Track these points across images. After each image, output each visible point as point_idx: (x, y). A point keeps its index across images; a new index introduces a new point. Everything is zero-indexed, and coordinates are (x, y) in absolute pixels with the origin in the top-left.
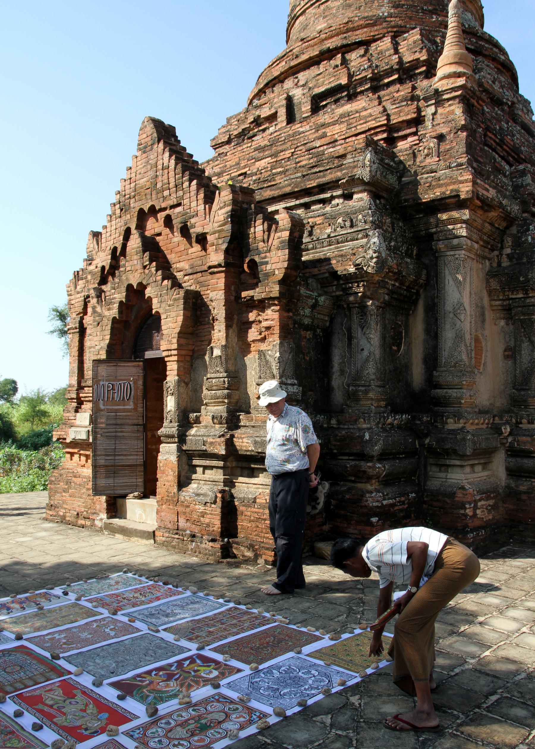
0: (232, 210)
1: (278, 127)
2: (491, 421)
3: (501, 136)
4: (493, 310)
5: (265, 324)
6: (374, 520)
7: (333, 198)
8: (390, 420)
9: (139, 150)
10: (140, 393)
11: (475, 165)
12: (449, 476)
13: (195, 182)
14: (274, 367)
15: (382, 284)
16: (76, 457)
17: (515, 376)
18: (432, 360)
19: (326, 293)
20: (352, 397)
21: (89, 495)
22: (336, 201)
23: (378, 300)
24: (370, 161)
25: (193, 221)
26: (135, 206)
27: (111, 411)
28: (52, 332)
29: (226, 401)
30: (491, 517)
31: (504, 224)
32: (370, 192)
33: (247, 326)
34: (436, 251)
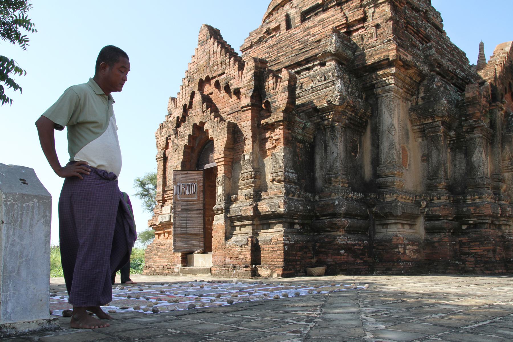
0: (255, 72)
1: (281, 33)
2: (414, 199)
3: (417, 27)
4: (414, 132)
5: (275, 138)
6: (342, 252)
7: (314, 66)
8: (350, 195)
9: (199, 44)
10: (201, 190)
11: (398, 41)
12: (388, 230)
13: (232, 59)
14: (281, 162)
15: (344, 113)
16: (162, 236)
17: (429, 172)
18: (376, 162)
19: (310, 121)
20: (328, 181)
21: (171, 254)
22: (316, 68)
23: (342, 123)
24: (335, 41)
25: (232, 82)
26: (197, 78)
27: (184, 201)
28: (136, 195)
29: (253, 185)
30: (415, 257)
31: (418, 79)
32: (336, 60)
33: (264, 141)
34: (377, 95)
